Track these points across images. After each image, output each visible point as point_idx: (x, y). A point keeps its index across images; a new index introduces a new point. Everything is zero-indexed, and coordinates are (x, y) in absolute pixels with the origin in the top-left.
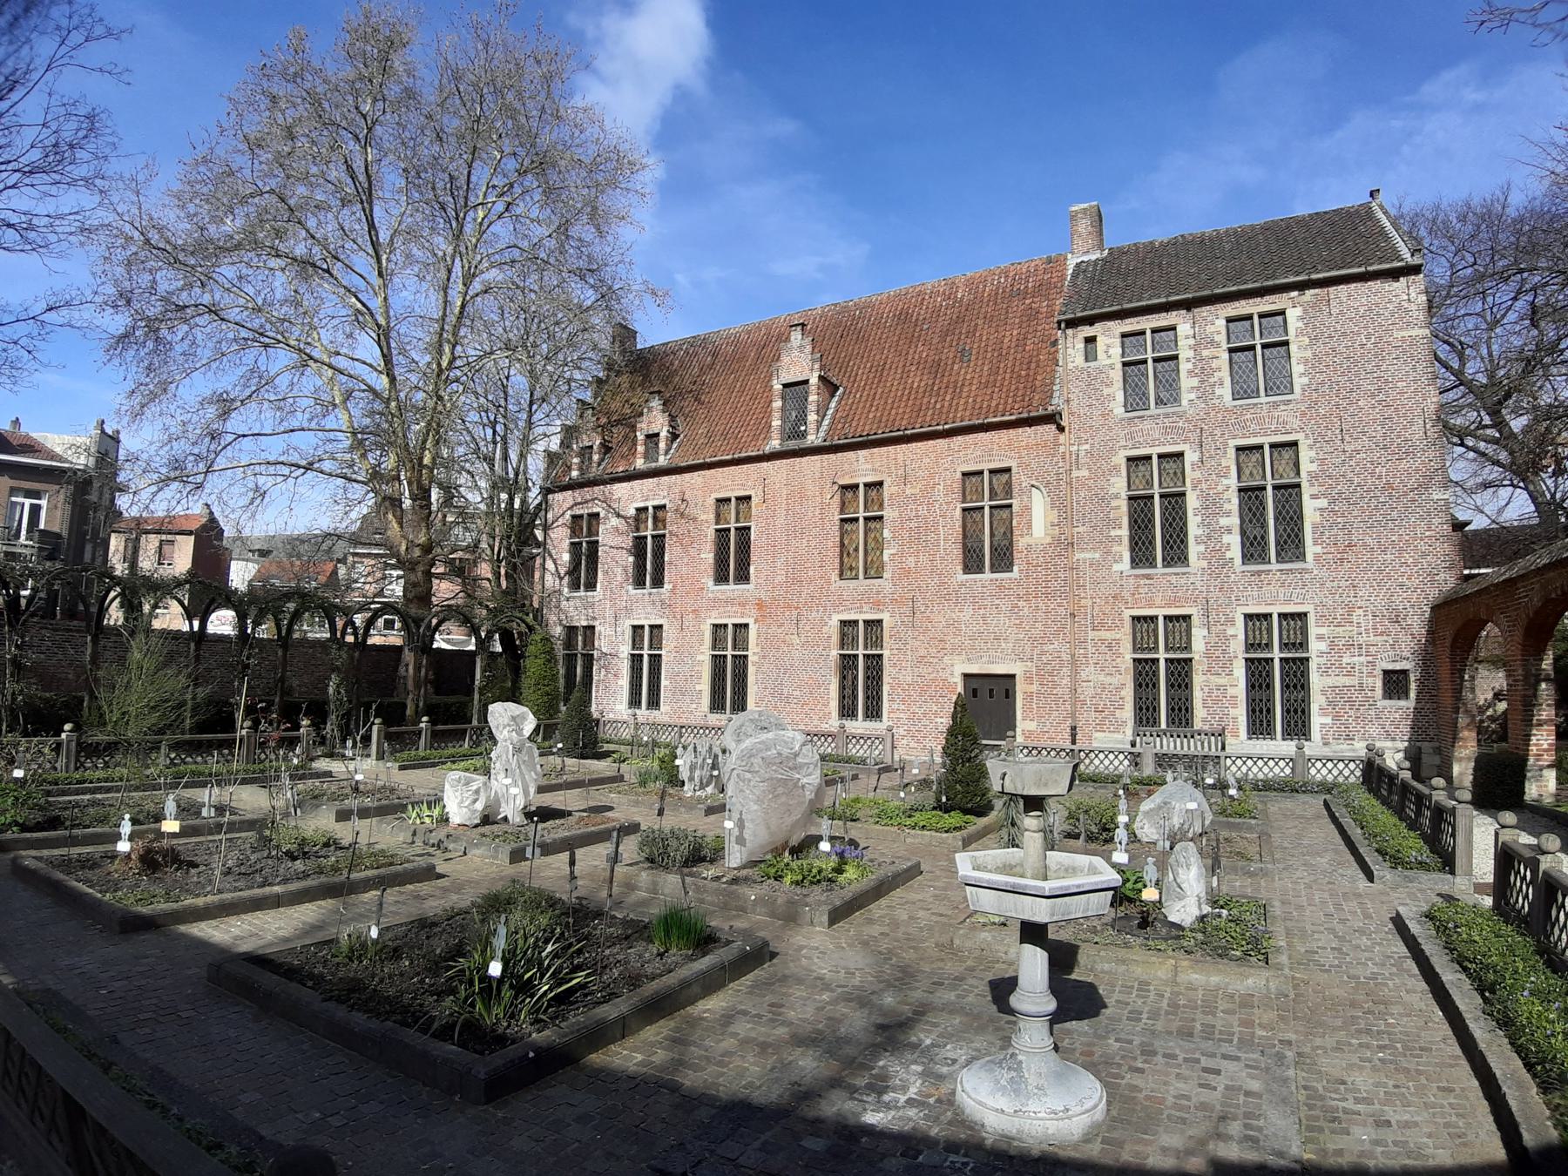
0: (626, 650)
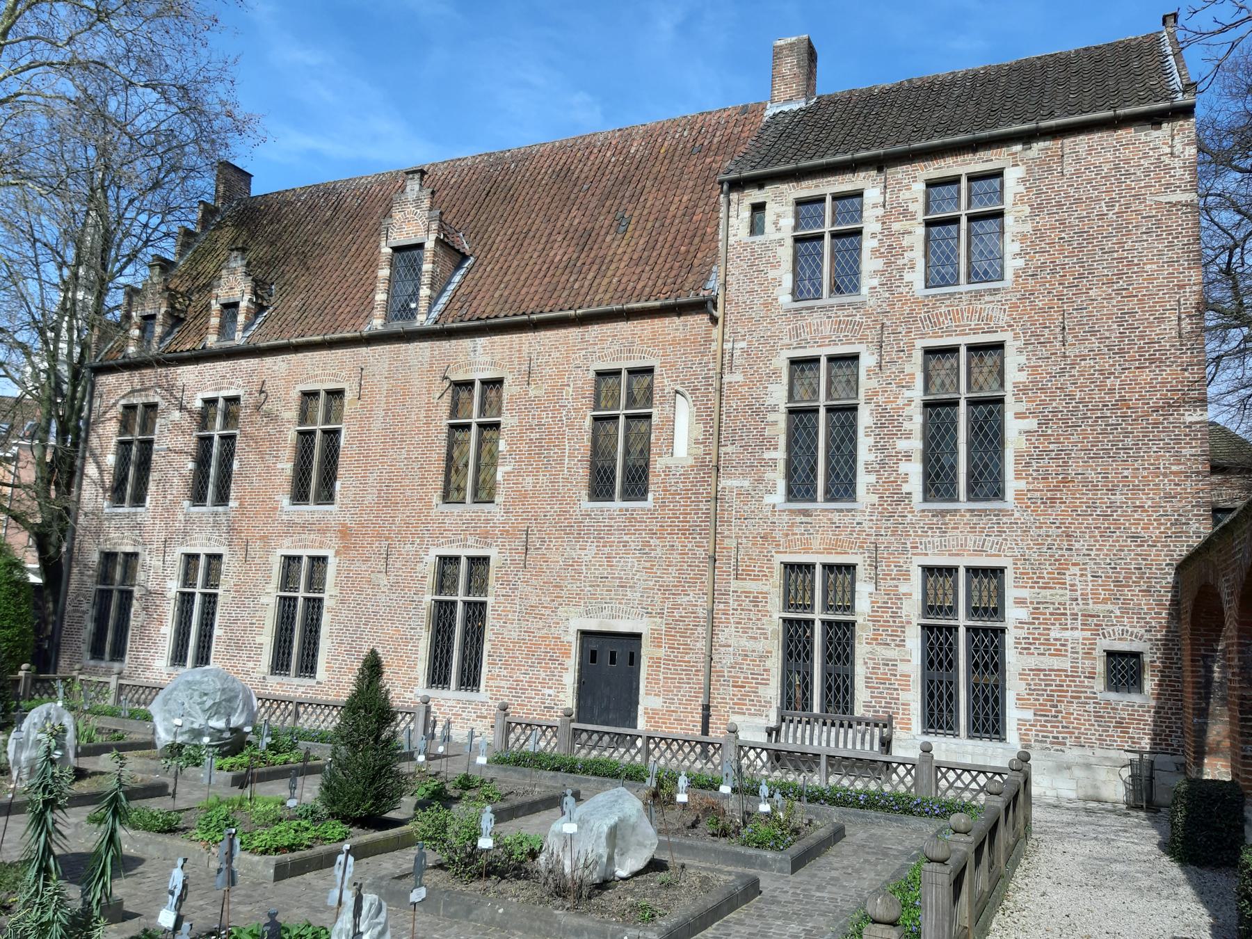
0: (174, 587)
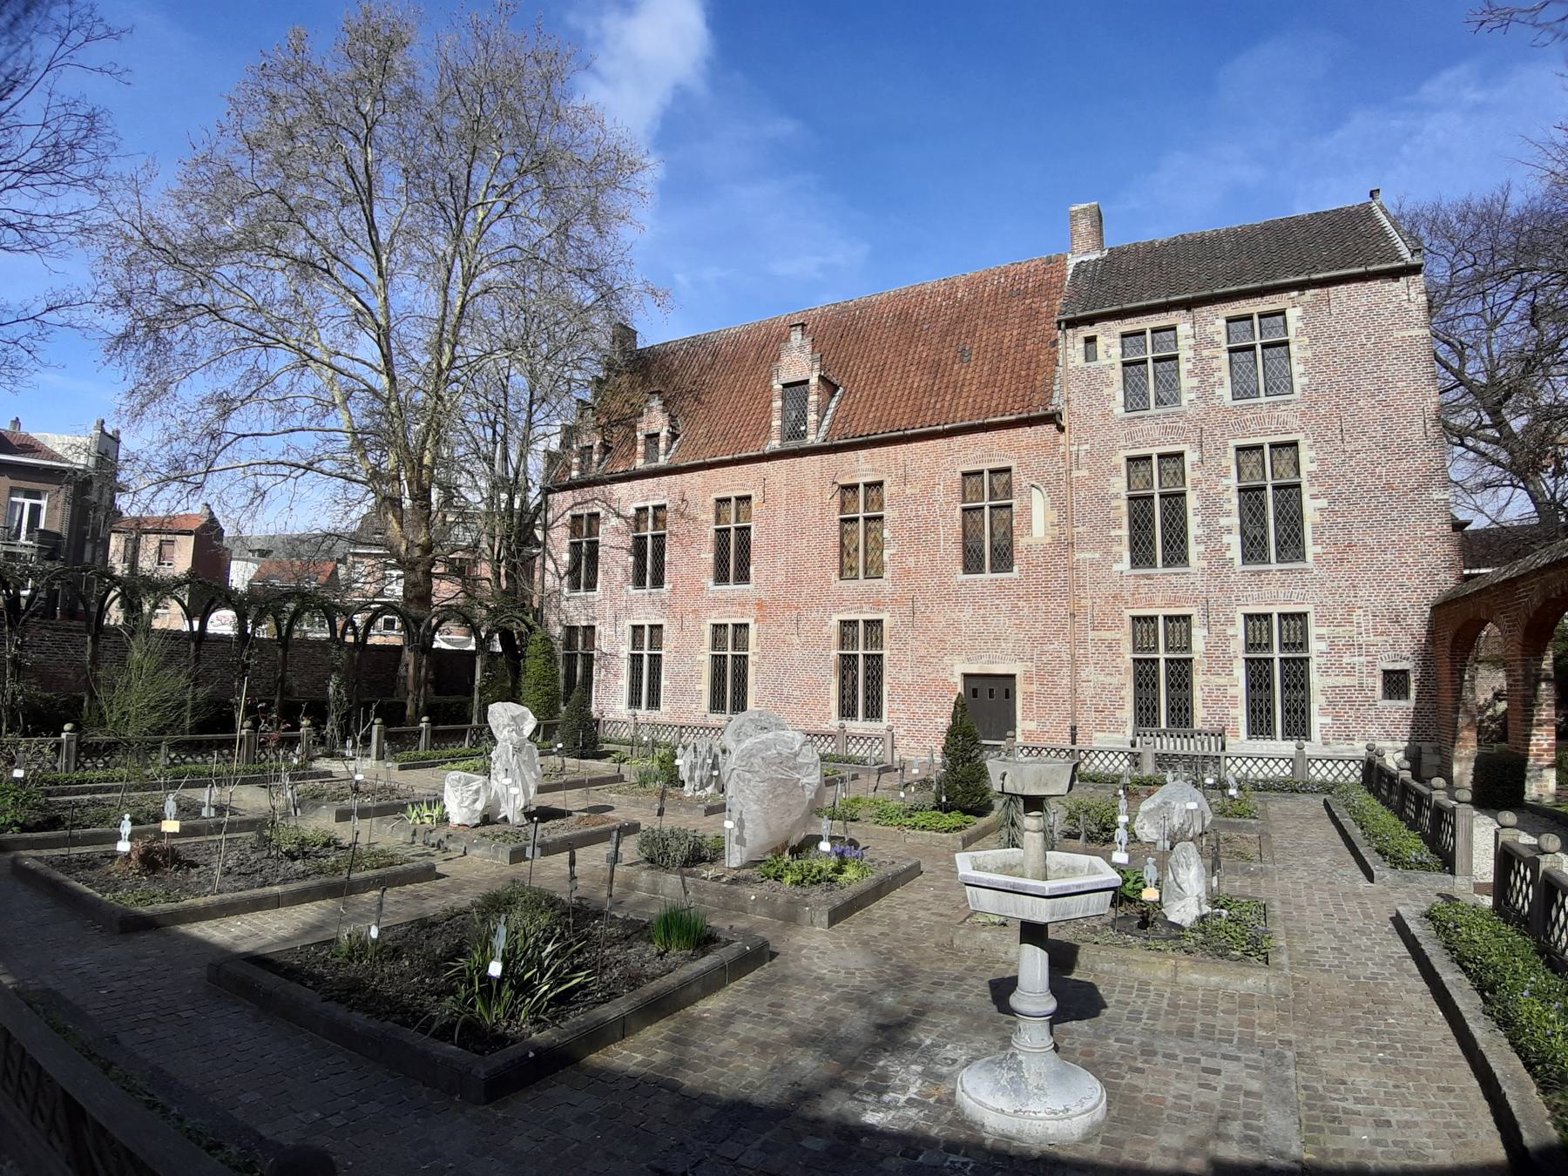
0: (626, 650)
